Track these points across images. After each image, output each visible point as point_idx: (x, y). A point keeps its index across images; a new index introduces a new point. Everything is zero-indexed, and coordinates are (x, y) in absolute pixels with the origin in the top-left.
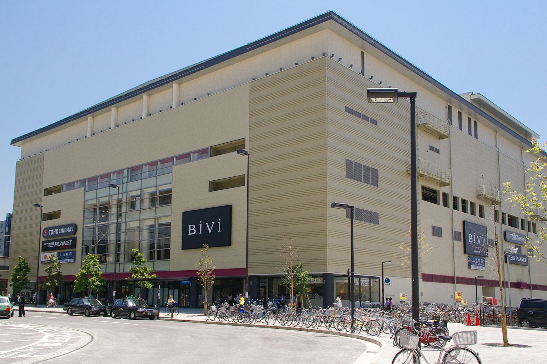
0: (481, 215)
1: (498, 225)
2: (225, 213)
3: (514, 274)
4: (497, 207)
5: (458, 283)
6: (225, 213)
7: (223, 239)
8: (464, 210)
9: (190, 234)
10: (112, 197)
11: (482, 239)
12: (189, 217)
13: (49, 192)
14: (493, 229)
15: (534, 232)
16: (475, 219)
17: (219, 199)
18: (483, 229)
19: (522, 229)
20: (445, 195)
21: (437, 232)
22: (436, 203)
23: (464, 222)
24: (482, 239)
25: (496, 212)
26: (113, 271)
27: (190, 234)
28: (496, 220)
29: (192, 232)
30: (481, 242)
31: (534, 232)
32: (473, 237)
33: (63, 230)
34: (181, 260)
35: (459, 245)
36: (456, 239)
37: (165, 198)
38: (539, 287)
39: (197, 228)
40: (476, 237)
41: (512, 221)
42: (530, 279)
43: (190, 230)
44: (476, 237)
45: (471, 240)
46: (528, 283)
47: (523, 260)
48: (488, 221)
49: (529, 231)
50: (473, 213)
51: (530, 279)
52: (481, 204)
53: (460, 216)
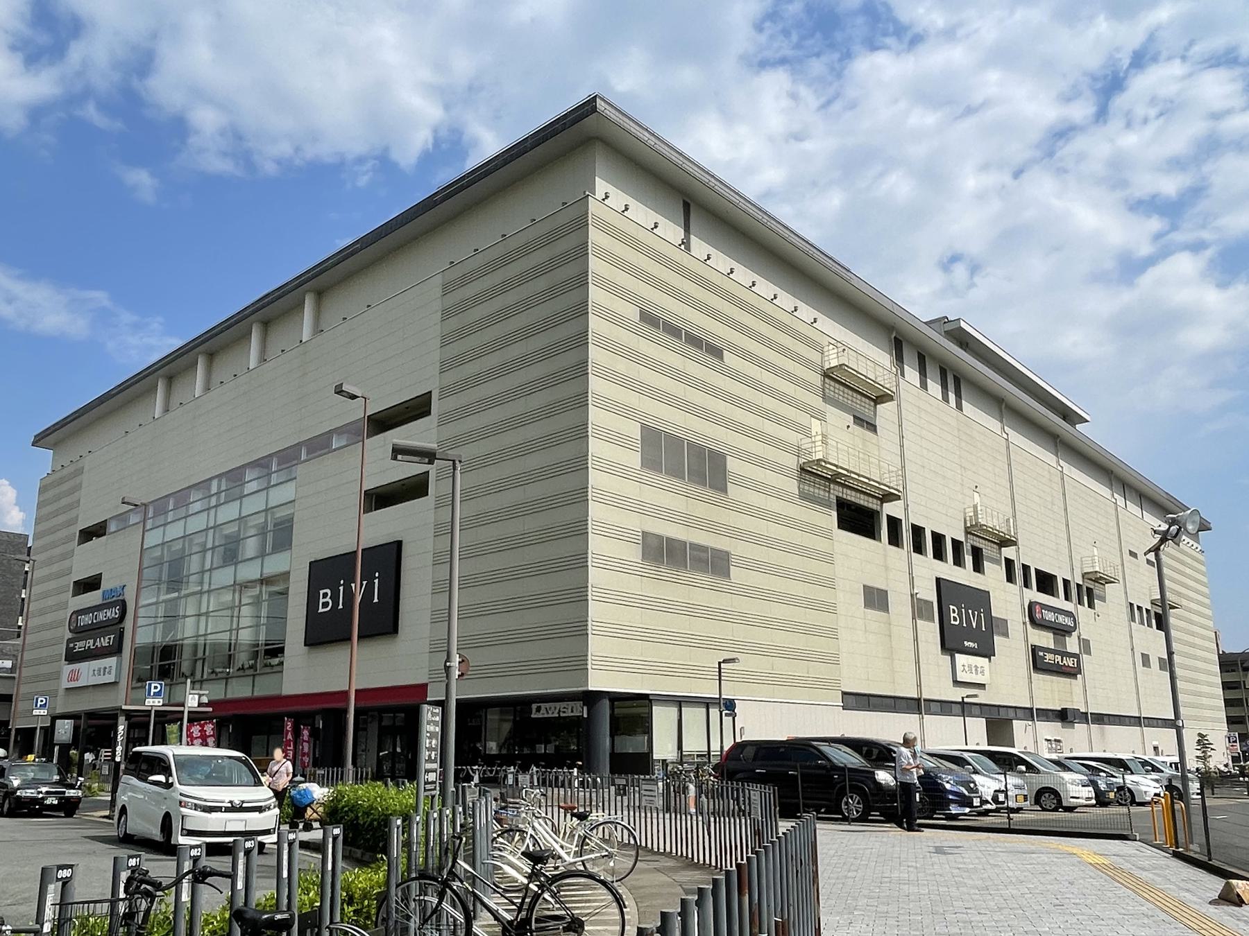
0: (978, 567)
1: (1014, 589)
2: (387, 559)
3: (1051, 691)
4: (1008, 552)
5: (929, 712)
6: (387, 559)
7: (383, 621)
8: (939, 555)
9: (321, 610)
10: (191, 540)
11: (979, 616)
12: (327, 572)
13: (88, 535)
14: (1009, 601)
15: (1091, 605)
16: (964, 576)
17: (383, 526)
18: (980, 599)
19: (1067, 598)
20: (894, 523)
21: (876, 599)
22: (874, 538)
23: (938, 580)
24: (979, 616)
25: (1009, 563)
26: (222, 697)
27: (321, 610)
28: (1010, 578)
29: (325, 605)
30: (979, 623)
31: (1090, 606)
32: (960, 614)
33: (102, 616)
34: (306, 673)
35: (930, 631)
36: (921, 617)
37: (281, 534)
38: (1106, 719)
39: (335, 598)
40: (967, 613)
41: (1046, 582)
42: (919, 686)
43: (322, 601)
44: (967, 613)
45: (955, 619)
46: (1083, 710)
47: (1070, 662)
48: (992, 579)
49: (1080, 602)
50: (958, 561)
51: (919, 686)
52: (977, 545)
53: (928, 569)
